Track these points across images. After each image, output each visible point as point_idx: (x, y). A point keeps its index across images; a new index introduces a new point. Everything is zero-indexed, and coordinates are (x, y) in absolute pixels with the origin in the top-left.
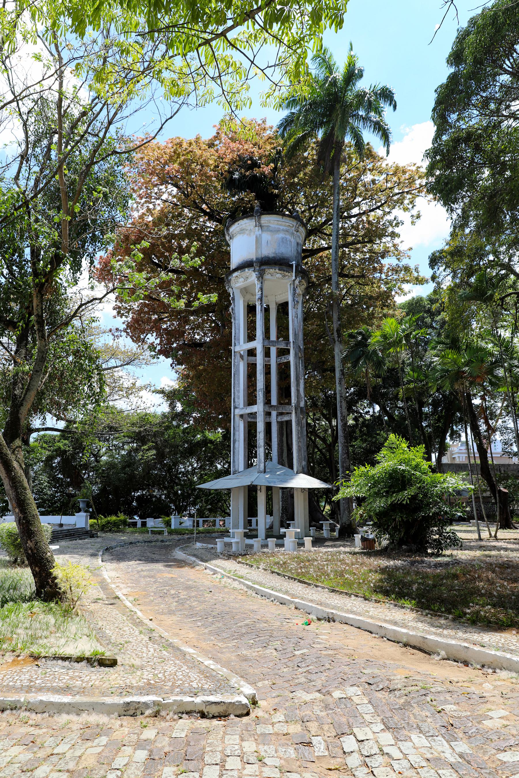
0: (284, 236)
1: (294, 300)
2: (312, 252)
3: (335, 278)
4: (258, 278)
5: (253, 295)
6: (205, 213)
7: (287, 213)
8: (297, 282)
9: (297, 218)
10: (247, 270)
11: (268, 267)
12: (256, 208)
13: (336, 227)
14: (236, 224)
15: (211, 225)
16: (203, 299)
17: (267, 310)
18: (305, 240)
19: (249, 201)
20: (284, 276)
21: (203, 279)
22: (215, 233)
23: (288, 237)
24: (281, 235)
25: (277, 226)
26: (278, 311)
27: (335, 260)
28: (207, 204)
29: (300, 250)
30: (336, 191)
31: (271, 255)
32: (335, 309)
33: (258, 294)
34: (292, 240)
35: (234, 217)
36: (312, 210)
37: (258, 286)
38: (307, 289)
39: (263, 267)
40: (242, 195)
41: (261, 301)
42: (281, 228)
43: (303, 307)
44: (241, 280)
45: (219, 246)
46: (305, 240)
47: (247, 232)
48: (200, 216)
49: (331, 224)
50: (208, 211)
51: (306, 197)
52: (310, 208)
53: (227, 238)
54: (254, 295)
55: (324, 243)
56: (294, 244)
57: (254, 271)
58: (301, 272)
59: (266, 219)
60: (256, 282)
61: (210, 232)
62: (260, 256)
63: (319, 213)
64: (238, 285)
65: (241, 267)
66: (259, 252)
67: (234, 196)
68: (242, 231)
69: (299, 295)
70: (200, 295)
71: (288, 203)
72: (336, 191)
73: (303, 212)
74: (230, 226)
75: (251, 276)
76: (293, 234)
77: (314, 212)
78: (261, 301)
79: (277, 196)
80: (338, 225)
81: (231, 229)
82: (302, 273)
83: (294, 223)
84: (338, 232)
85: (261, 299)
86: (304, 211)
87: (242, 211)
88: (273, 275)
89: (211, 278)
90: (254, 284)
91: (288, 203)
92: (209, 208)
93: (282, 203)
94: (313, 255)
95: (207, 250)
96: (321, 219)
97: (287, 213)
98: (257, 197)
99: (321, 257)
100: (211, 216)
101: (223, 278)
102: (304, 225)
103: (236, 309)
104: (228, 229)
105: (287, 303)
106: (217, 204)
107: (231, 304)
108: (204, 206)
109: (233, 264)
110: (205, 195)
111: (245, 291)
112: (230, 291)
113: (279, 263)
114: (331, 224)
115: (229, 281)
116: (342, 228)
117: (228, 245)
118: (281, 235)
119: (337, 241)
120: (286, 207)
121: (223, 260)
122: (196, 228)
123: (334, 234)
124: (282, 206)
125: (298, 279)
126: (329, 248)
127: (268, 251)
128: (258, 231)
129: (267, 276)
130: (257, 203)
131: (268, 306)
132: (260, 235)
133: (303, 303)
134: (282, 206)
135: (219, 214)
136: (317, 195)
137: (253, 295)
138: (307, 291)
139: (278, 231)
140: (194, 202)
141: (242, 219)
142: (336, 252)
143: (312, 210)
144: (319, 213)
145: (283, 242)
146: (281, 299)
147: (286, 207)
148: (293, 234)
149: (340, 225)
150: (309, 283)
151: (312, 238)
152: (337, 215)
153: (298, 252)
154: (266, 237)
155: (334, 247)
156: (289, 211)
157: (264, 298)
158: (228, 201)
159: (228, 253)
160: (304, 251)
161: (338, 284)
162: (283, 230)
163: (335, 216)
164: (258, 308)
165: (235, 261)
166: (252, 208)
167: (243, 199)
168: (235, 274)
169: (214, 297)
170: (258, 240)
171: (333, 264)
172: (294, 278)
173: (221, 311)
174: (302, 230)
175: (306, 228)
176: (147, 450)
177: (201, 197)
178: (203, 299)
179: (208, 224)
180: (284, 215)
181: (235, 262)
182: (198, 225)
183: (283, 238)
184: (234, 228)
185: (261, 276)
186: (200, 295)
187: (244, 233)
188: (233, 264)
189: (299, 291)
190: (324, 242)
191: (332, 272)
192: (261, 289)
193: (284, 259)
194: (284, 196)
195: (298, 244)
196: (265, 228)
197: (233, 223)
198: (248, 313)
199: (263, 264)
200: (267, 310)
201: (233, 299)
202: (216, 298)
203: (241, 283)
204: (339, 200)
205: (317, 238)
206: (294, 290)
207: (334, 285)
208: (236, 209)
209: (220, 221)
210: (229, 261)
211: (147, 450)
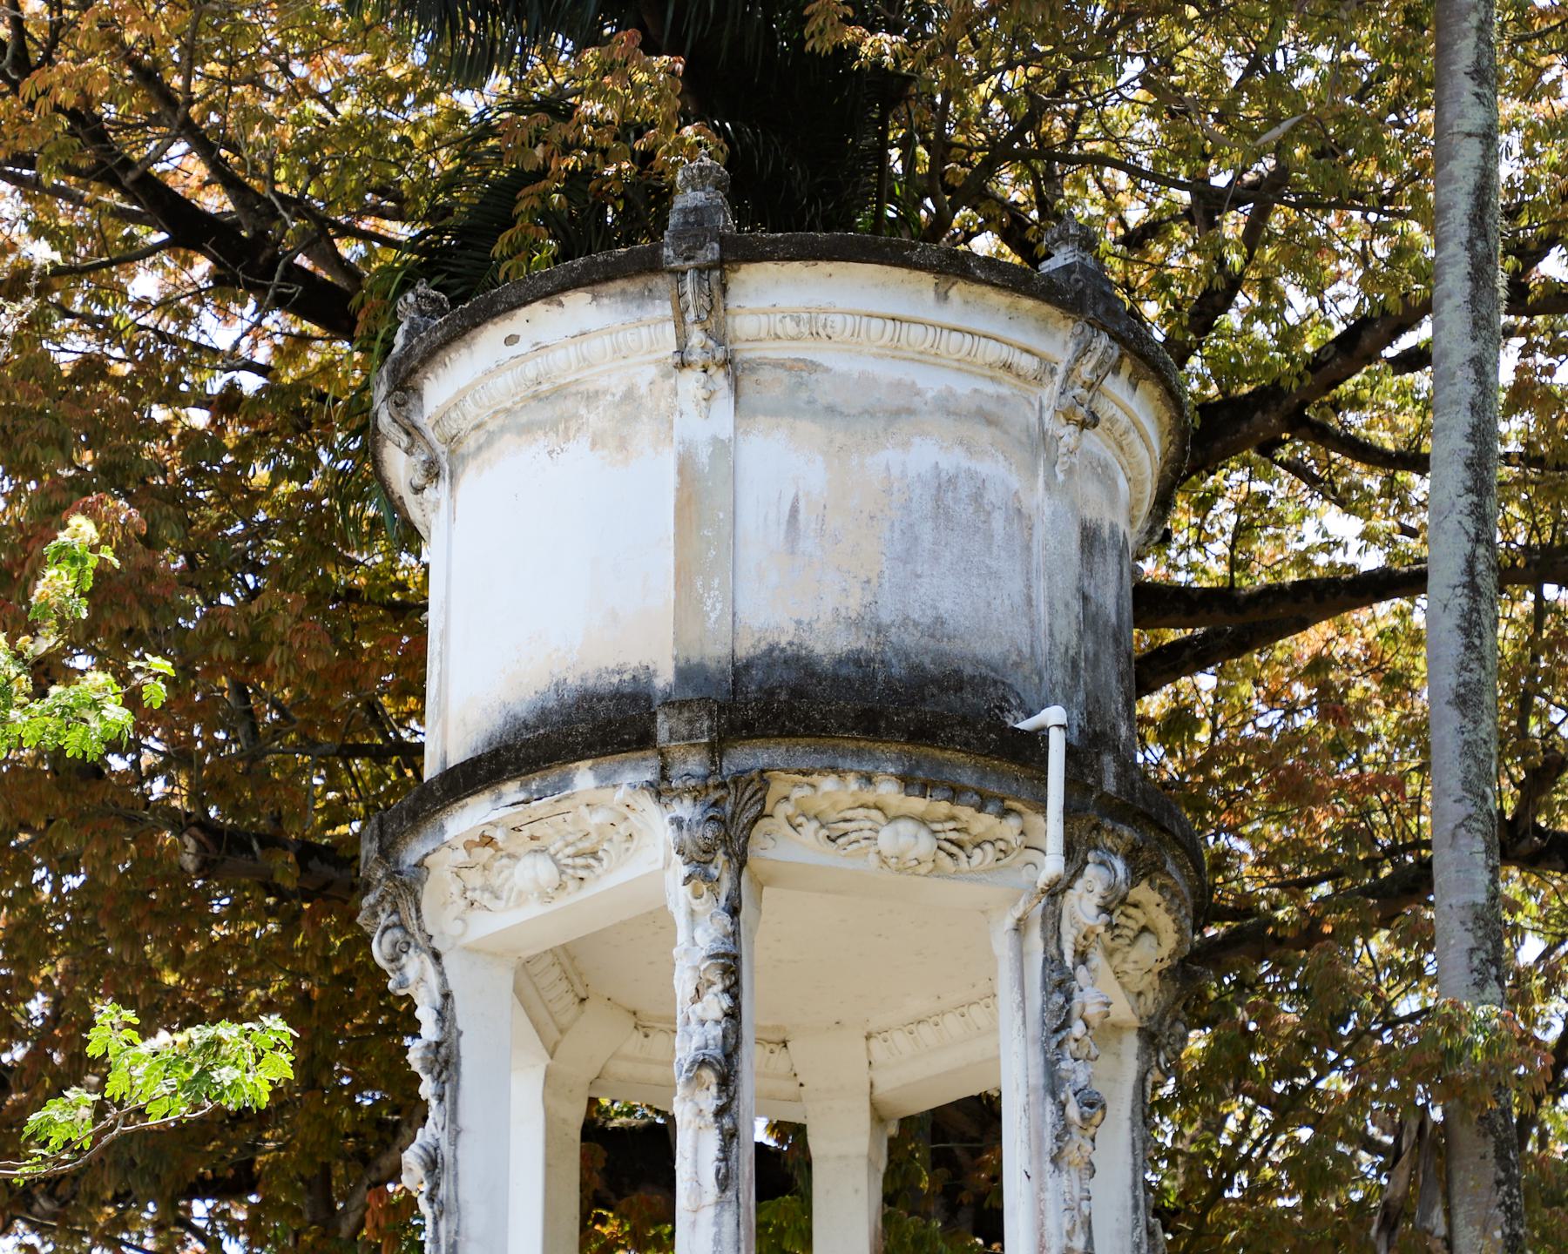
0: (953, 460)
1: (1053, 1084)
2: (1240, 620)
3: (1462, 873)
4: (699, 862)
5: (641, 1023)
6: (187, 228)
7: (985, 244)
8: (1083, 906)
9: (1086, 300)
10: (584, 776)
11: (801, 752)
12: (687, 199)
13: (1464, 386)
14: (491, 337)
15: (238, 333)
16: (147, 1067)
17: (781, 1176)
18: (1164, 503)
19: (629, 129)
20: (957, 846)
21: (151, 865)
22: (292, 414)
23: (999, 471)
24: (925, 454)
25: (889, 371)
26: (897, 1194)
27: (1466, 700)
28: (204, 145)
29: (1111, 597)
30: (1465, 53)
31: (830, 641)
32: (1475, 1174)
33: (696, 1023)
34: (1038, 500)
35: (477, 259)
36: (1233, 224)
37: (696, 935)
38: (1186, 971)
39: (745, 757)
40: (558, 65)
41: (727, 1080)
42: (932, 383)
43: (1147, 1152)
44: (531, 872)
45: (321, 534)
46: (1164, 503)
47: (596, 418)
48: (133, 254)
49: (1415, 359)
50: (215, 201)
51: (1169, 103)
52: (1208, 206)
53: (399, 466)
54: (648, 1022)
55: (1336, 536)
56: (1056, 542)
57: (660, 790)
58: (1121, 810)
59: (781, 298)
60: (678, 897)
61: (229, 403)
62: (714, 651)
63: (1307, 260)
64: (489, 924)
65: (534, 750)
66: (715, 609)
67: (471, 73)
68: (547, 406)
69: (1107, 1031)
70: (110, 1028)
71: (999, 152)
72: (1465, 53)
73: (1136, 240)
74: (430, 354)
75: (627, 838)
76: (1042, 442)
77: (1254, 236)
78: (727, 1080)
79: (889, 88)
80: (1482, 367)
81: (441, 389)
82: (1138, 820)
83: (1057, 340)
84: (1483, 435)
85: (724, 1068)
86: (1153, 229)
87: (548, 217)
88: (847, 830)
89: (223, 849)
90: (658, 921)
91: (999, 152)
92: (222, 175)
93: (942, 149)
94: (1241, 644)
95: (192, 578)
96: (1323, 307)
97: (985, 244)
98: (703, 95)
99: (1320, 664)
100: (244, 257)
101: (342, 856)
102: (1154, 365)
103: (470, 1161)
104: (405, 386)
105: (981, 1114)
106: (308, 147)
107: (415, 1112)
108: (182, 167)
109: (450, 729)
110: (193, 55)
111: (568, 982)
112: (416, 978)
113: (916, 717)
114: (1415, 359)
115: (408, 886)
116: (1524, 394)
117: (411, 538)
118: (925, 454)
119: (1481, 516)
120: (977, 192)
121: (350, 670)
122: (91, 368)
123: (1449, 446)
124: (936, 183)
125: (1095, 881)
126: (1401, 582)
127: (797, 602)
128: (698, 412)
129: (783, 845)
130: (694, 159)
131: (792, 1132)
132: (723, 448)
133: (1148, 1110)
134: (936, 183)
135: (320, 237)
136: (1278, 84)
137: (641, 1023)
138: (1188, 986)
139: (898, 413)
140: (84, 121)
141: (551, 291)
142: (1473, 627)
143: (1233, 224)
144: (1307, 260)
145: (942, 514)
146: (927, 1076)
147: (977, 192)
148: (1042, 442)
149: (1506, 375)
150: (1205, 912)
151: (1234, 480)
152: (1480, 274)
153: (1090, 620)
154: (779, 463)
155: (1446, 572)
156: (1013, 230)
157: (751, 1059)
158: (413, 119)
159: (407, 611)
160: (1153, 602)
161: (1493, 928)
162: (948, 408)
163: (1455, 283)
164: (696, 1156)
165: (469, 691)
166: (649, 197)
167: (557, 108)
168: (471, 816)
169: (254, 1060)
170: (700, 498)
171: (1448, 734)
172: (1053, 864)
173: (320, 1186)
174: (1133, 408)
175: (1172, 395)
176: (1248, 1120)
177: (149, 77)
178: (147, 1067)
179: (216, 331)
180: (958, 268)
181: (461, 706)
182: (106, 330)
183: (943, 485)
184: (473, 377)
185: (726, 842)
186: (110, 1028)
187: (562, 427)
188: (450, 729)
189: (1112, 992)
190: (1346, 526)
191: (1438, 813)
192: (730, 966)
193: (954, 681)
194: (958, 88)
195: (1090, 538)
196: (768, 387)
197: (460, 331)
198: (593, 1201)
199: (748, 726)
200: (781, 1176)
201: (445, 1061)
202: (281, 1067)
203: (528, 924)
204: (1488, 137)
205: (1280, 488)
206: (1059, 982)
207: (1456, 938)
208: (497, 210)
209: (329, 305)
210: (412, 683)
211: (1248, 1120)
